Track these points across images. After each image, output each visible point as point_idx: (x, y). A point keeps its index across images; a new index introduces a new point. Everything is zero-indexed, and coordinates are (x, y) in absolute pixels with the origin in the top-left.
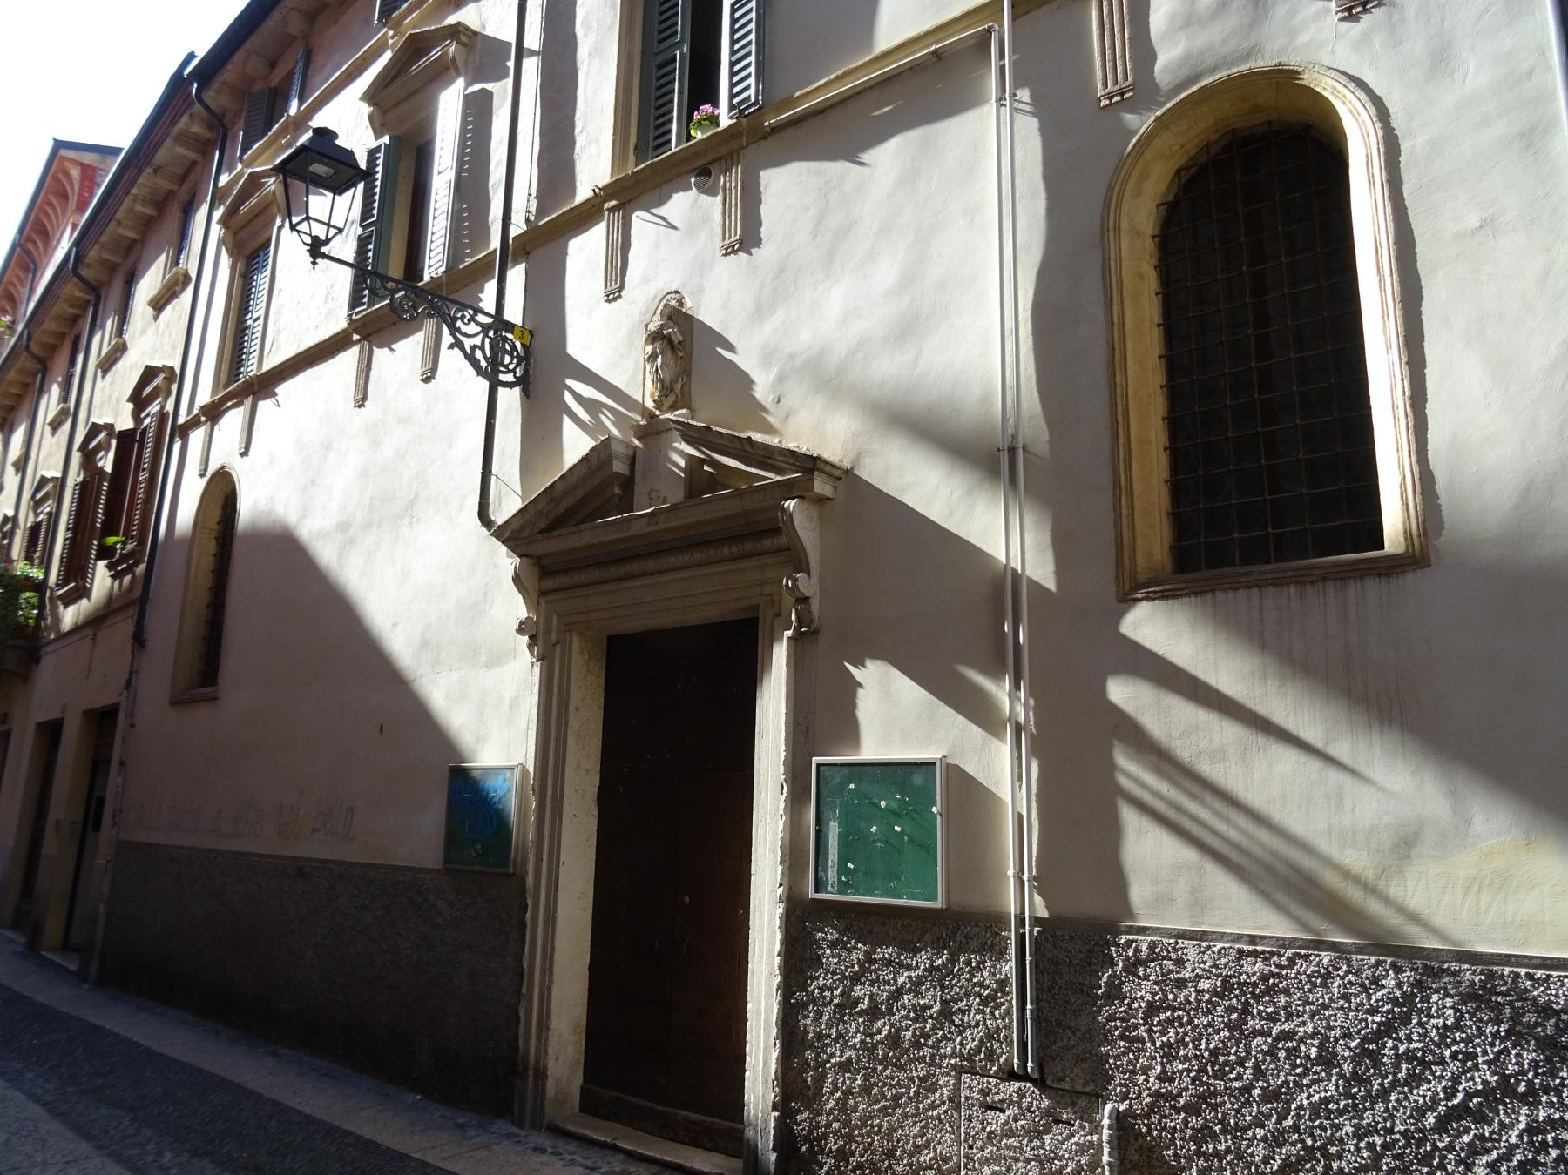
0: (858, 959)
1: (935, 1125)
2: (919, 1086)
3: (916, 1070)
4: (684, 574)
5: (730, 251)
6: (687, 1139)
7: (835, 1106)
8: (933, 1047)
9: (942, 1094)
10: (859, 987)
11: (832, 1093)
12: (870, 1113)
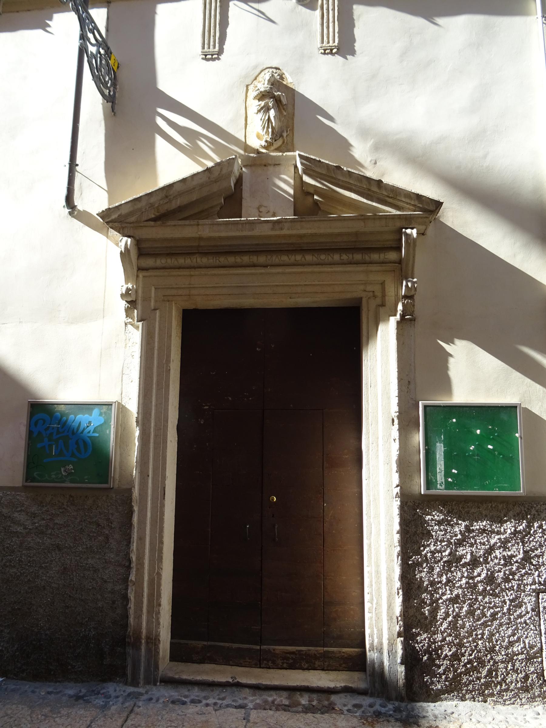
0: (460, 531)
1: (523, 627)
2: (510, 605)
3: (507, 595)
4: (317, 269)
5: (328, 52)
6: (285, 665)
7: (448, 626)
8: (519, 580)
9: (526, 608)
10: (462, 548)
11: (444, 619)
12: (474, 627)
